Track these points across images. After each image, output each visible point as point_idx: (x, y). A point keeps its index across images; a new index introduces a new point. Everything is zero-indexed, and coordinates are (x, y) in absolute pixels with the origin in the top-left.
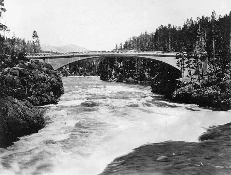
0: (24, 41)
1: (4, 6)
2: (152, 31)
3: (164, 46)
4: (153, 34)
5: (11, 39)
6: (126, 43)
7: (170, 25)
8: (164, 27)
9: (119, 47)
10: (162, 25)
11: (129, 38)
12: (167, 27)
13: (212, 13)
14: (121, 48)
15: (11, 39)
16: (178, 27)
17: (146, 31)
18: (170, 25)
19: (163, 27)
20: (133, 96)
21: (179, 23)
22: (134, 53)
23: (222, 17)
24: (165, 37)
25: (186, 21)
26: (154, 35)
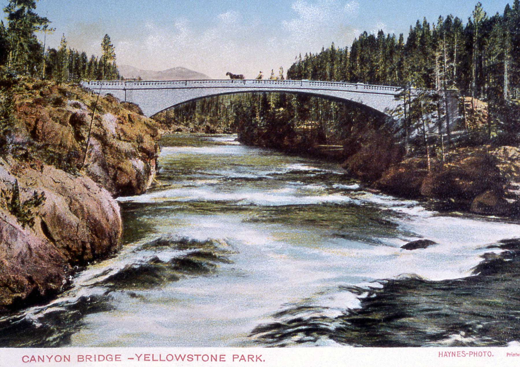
0: (84, 54)
1: (401, 33)
2: (344, 43)
3: (371, 73)
4: (346, 52)
5: (465, 24)
6: (293, 67)
7: (381, 33)
8: (368, 35)
9: (277, 75)
10: (365, 32)
11: (298, 56)
12: (376, 37)
13: (474, 8)
14: (282, 78)
15: (465, 24)
16: (397, 38)
17: (333, 43)
18: (381, 33)
19: (367, 34)
20: (308, 175)
21: (397, 27)
22: (306, 86)
23: (489, 19)
24: (369, 59)
25: (414, 26)
26: (349, 50)
